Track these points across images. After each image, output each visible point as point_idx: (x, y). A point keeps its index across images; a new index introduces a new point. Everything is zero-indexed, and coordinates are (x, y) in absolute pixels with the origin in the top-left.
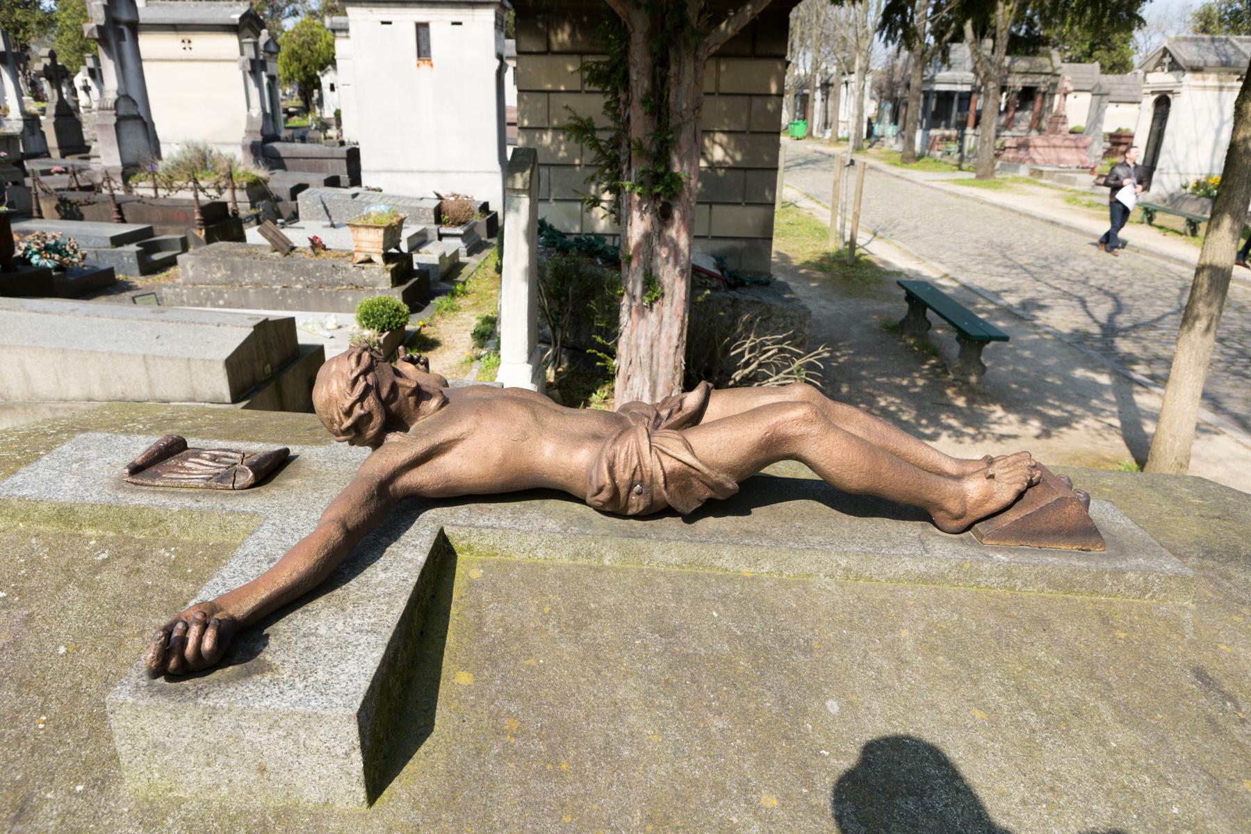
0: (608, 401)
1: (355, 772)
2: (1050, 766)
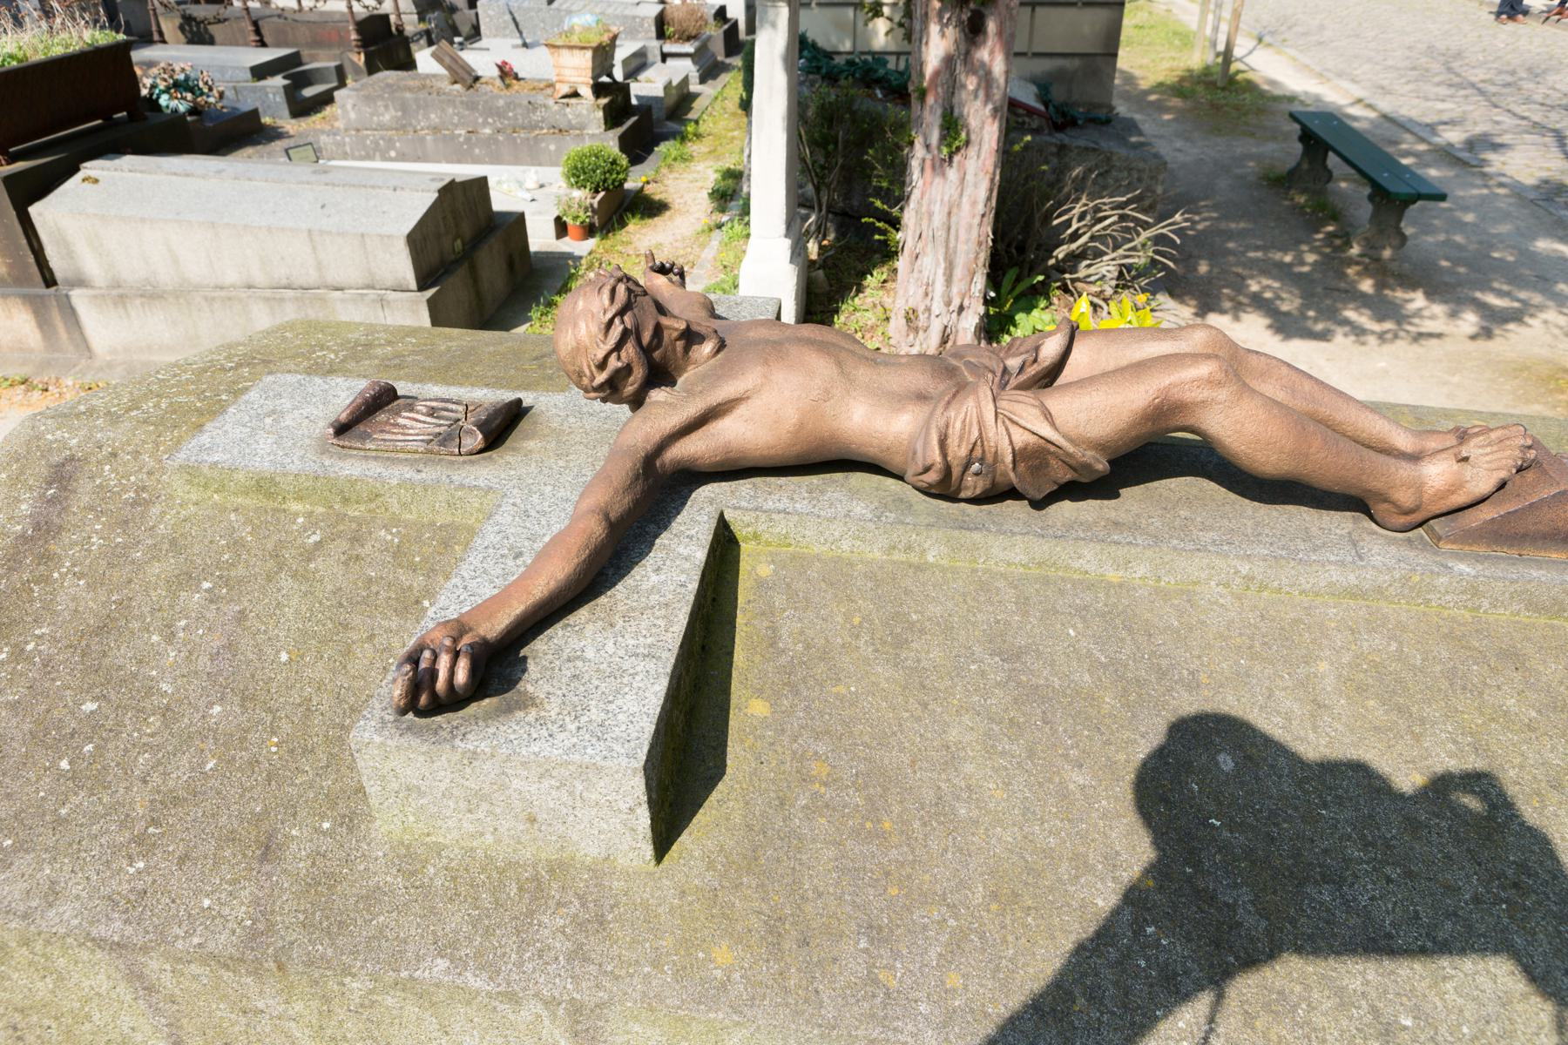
0: (888, 285)
2: (1515, 854)
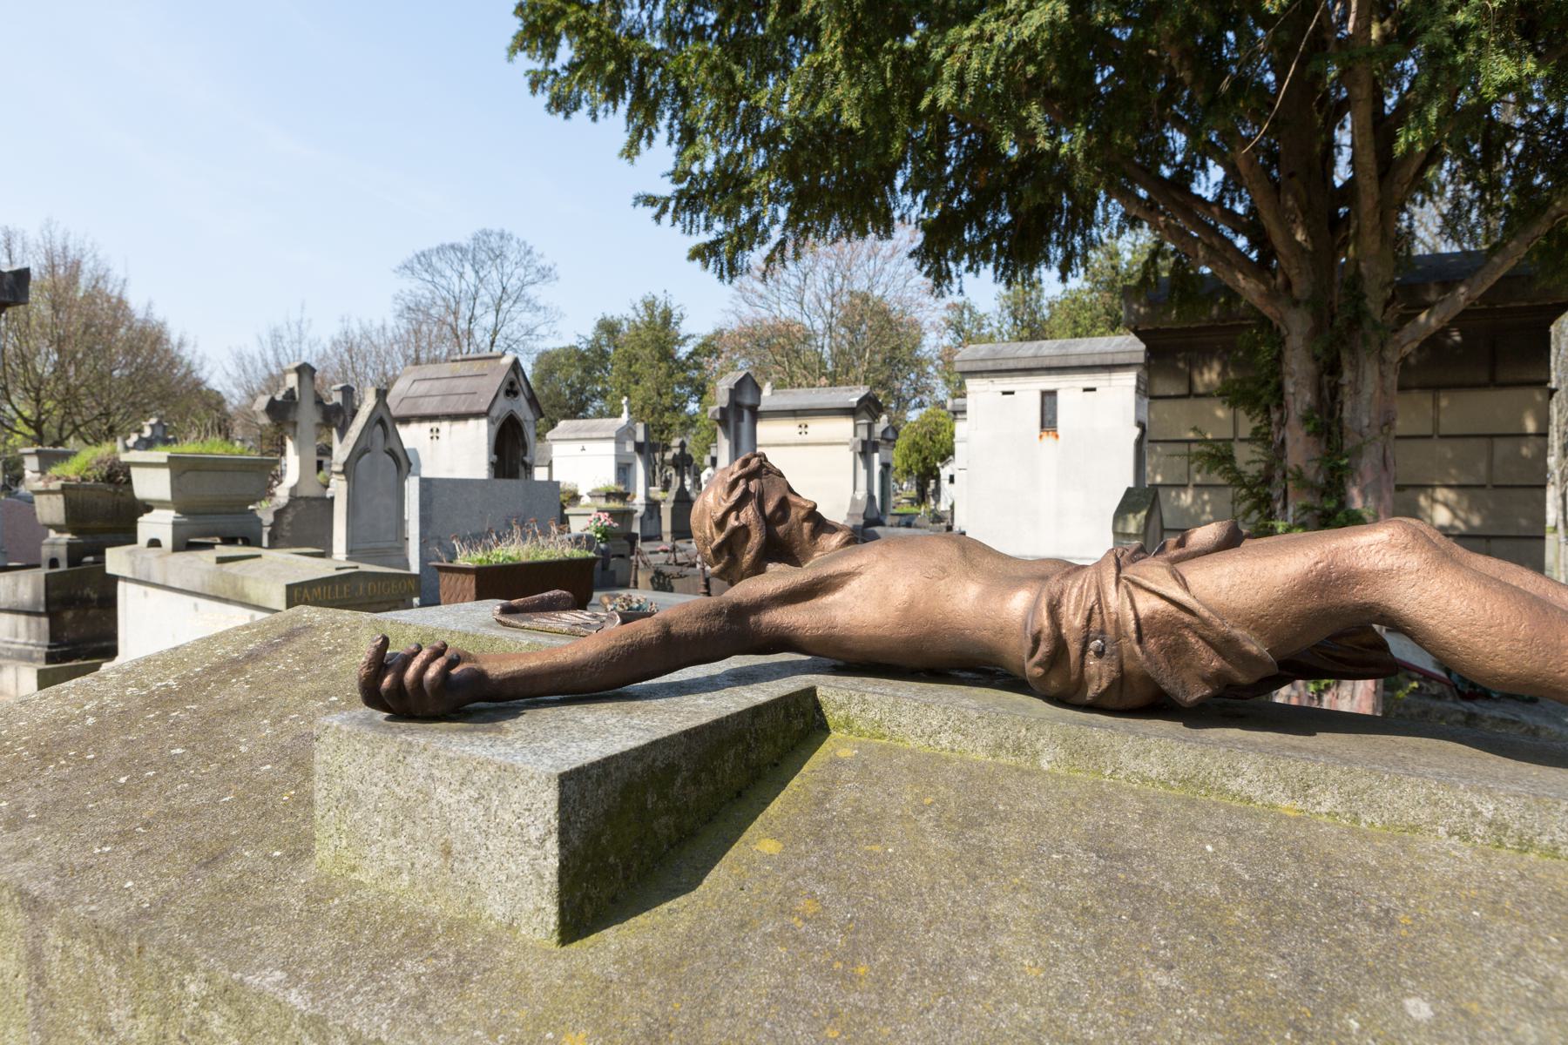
1: (547, 873)
